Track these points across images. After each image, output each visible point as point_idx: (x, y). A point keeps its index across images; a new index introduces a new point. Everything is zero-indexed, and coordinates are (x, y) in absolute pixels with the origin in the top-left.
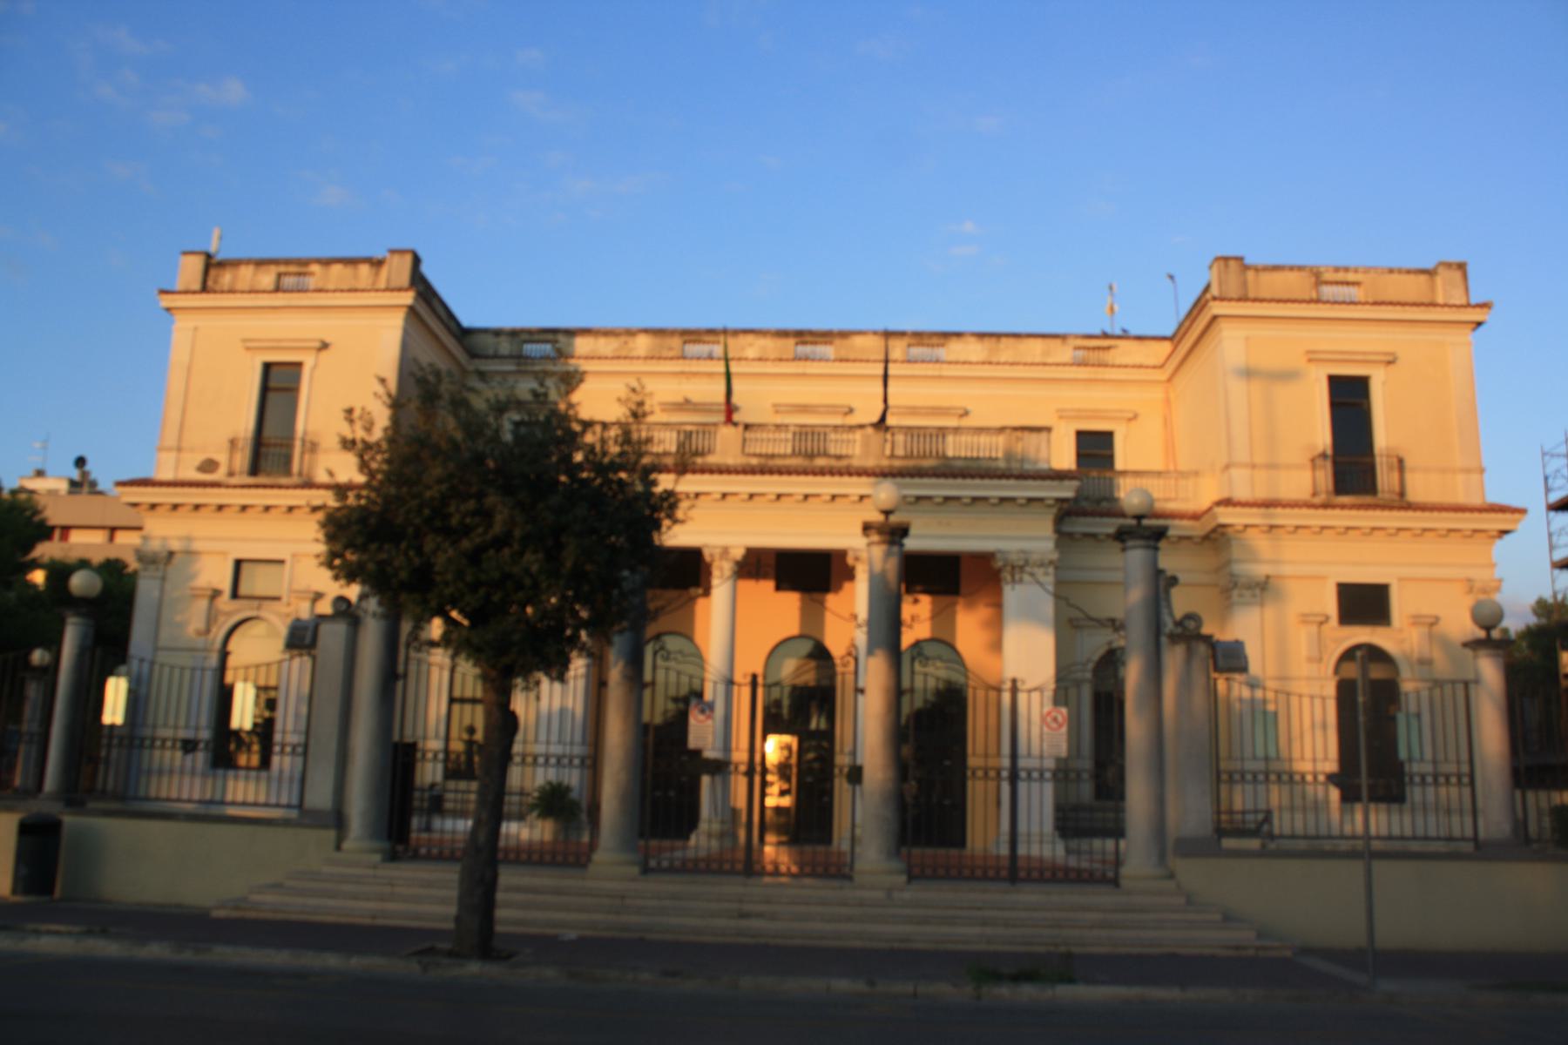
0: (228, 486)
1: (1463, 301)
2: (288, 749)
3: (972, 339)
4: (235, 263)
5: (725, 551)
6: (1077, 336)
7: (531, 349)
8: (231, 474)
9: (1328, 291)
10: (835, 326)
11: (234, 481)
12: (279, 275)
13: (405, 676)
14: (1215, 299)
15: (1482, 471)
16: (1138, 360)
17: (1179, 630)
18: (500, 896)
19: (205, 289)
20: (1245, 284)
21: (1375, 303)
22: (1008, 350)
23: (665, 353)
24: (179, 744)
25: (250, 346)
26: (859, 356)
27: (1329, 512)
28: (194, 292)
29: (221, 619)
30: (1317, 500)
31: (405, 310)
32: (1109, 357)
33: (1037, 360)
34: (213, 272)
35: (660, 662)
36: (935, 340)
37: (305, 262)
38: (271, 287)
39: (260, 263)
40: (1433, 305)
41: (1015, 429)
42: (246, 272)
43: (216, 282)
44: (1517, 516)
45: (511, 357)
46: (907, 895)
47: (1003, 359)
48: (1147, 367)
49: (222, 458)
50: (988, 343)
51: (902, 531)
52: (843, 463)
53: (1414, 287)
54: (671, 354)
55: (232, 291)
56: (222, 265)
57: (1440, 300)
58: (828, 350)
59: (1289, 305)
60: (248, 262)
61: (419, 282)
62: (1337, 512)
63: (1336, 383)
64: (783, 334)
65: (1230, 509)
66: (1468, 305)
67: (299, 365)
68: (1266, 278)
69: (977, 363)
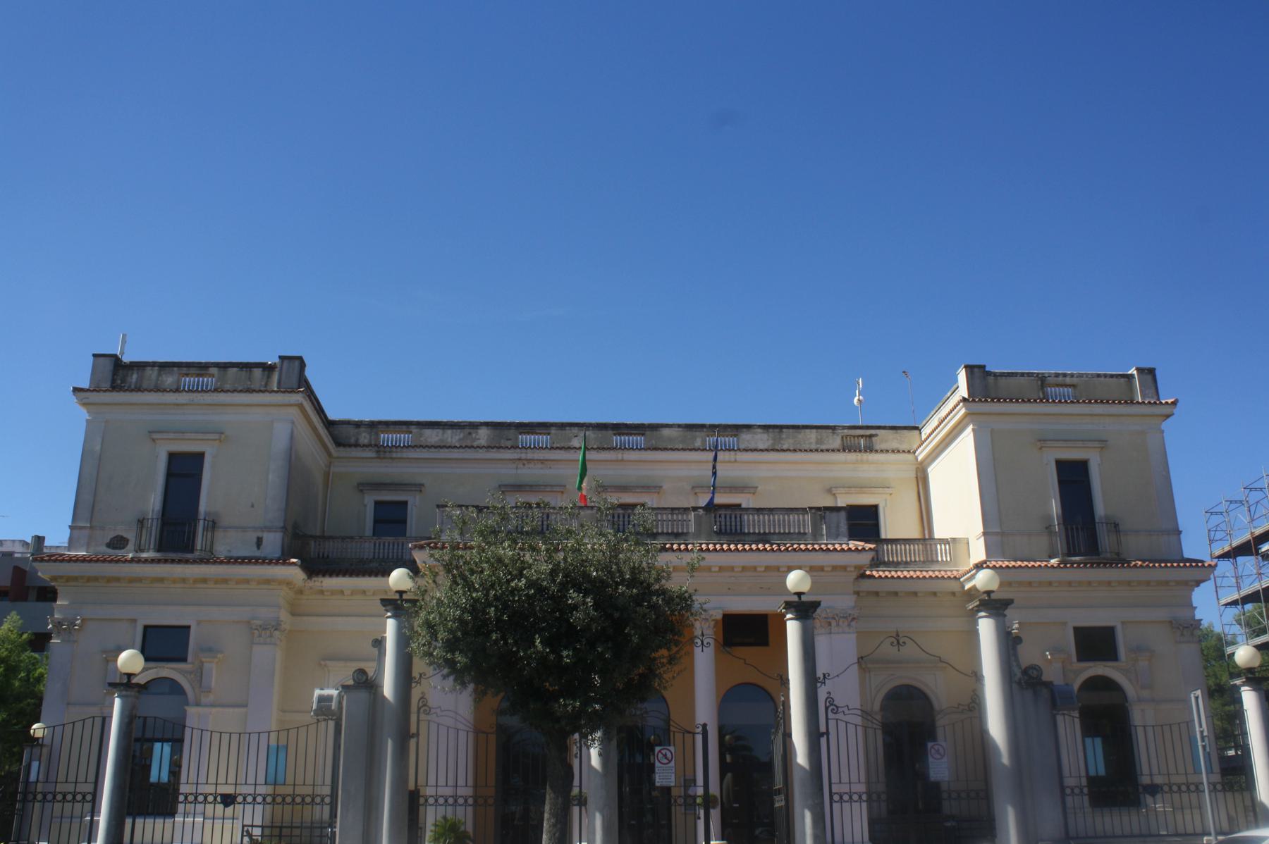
2: (259, 799)
3: (759, 430)
6: (844, 428)
7: (386, 438)
13: (417, 735)
15: (1180, 532)
22: (788, 441)
24: (219, 799)
25: (1043, 441)
33: (813, 447)
35: (831, 715)
41: (819, 509)
43: (123, 381)
45: (370, 445)
47: (785, 447)
49: (131, 536)
50: (772, 433)
55: (138, 389)
63: (1061, 465)
67: (200, 456)
68: (1002, 381)
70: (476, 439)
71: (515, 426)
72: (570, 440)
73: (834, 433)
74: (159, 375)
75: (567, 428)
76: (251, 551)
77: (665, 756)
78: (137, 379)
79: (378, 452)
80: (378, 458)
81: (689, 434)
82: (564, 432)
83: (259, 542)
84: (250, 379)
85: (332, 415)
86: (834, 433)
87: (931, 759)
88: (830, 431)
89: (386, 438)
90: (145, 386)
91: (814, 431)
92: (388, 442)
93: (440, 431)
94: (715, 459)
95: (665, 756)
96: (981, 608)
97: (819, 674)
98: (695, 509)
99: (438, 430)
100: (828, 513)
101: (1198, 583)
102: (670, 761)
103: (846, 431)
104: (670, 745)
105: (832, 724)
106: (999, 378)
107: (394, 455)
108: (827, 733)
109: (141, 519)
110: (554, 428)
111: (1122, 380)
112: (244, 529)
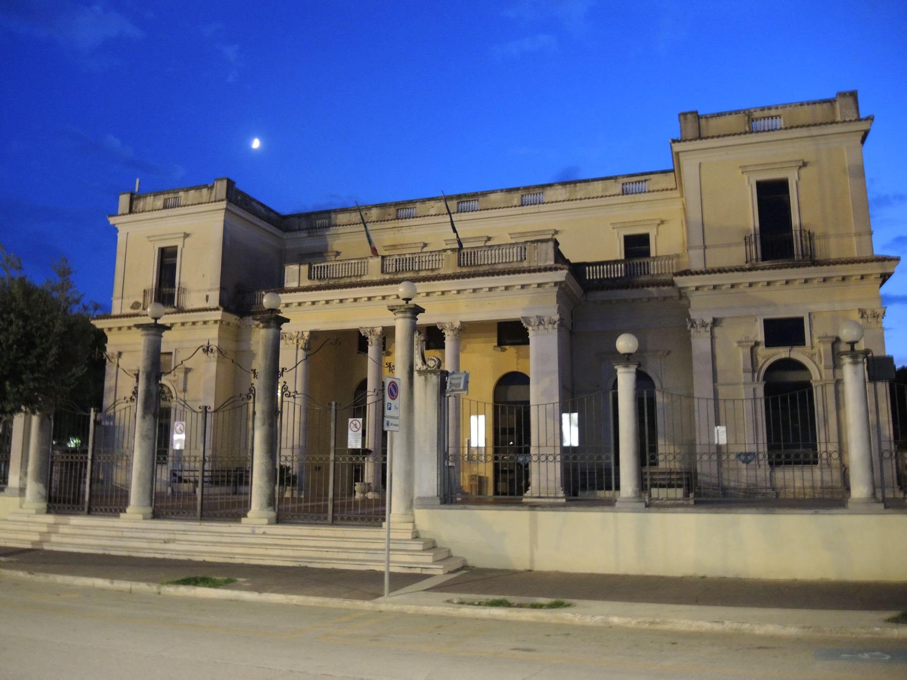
5: (372, 330)
6: (624, 176)
9: (760, 124)
10: (479, 189)
15: (871, 233)
17: (425, 367)
19: (131, 211)
23: (387, 217)
27: (754, 272)
28: (126, 214)
30: (747, 266)
31: (224, 211)
33: (600, 195)
34: (135, 203)
36: (537, 191)
40: (834, 122)
44: (893, 262)
47: (578, 197)
51: (417, 310)
52: (435, 273)
53: (820, 112)
54: (390, 217)
57: (839, 119)
59: (726, 138)
62: (759, 272)
66: (859, 120)
68: (713, 122)
69: (564, 201)
72: (428, 210)
73: (615, 182)
74: (154, 201)
76: (204, 305)
78: (143, 205)
79: (309, 233)
80: (309, 237)
82: (424, 205)
84: (201, 196)
86: (615, 182)
88: (613, 180)
90: (147, 209)
91: (601, 182)
94: (452, 222)
96: (408, 310)
98: (445, 250)
100: (539, 244)
102: (359, 429)
104: (183, 421)
105: (285, 404)
106: (709, 119)
107: (319, 234)
111: (825, 106)
112: (199, 291)
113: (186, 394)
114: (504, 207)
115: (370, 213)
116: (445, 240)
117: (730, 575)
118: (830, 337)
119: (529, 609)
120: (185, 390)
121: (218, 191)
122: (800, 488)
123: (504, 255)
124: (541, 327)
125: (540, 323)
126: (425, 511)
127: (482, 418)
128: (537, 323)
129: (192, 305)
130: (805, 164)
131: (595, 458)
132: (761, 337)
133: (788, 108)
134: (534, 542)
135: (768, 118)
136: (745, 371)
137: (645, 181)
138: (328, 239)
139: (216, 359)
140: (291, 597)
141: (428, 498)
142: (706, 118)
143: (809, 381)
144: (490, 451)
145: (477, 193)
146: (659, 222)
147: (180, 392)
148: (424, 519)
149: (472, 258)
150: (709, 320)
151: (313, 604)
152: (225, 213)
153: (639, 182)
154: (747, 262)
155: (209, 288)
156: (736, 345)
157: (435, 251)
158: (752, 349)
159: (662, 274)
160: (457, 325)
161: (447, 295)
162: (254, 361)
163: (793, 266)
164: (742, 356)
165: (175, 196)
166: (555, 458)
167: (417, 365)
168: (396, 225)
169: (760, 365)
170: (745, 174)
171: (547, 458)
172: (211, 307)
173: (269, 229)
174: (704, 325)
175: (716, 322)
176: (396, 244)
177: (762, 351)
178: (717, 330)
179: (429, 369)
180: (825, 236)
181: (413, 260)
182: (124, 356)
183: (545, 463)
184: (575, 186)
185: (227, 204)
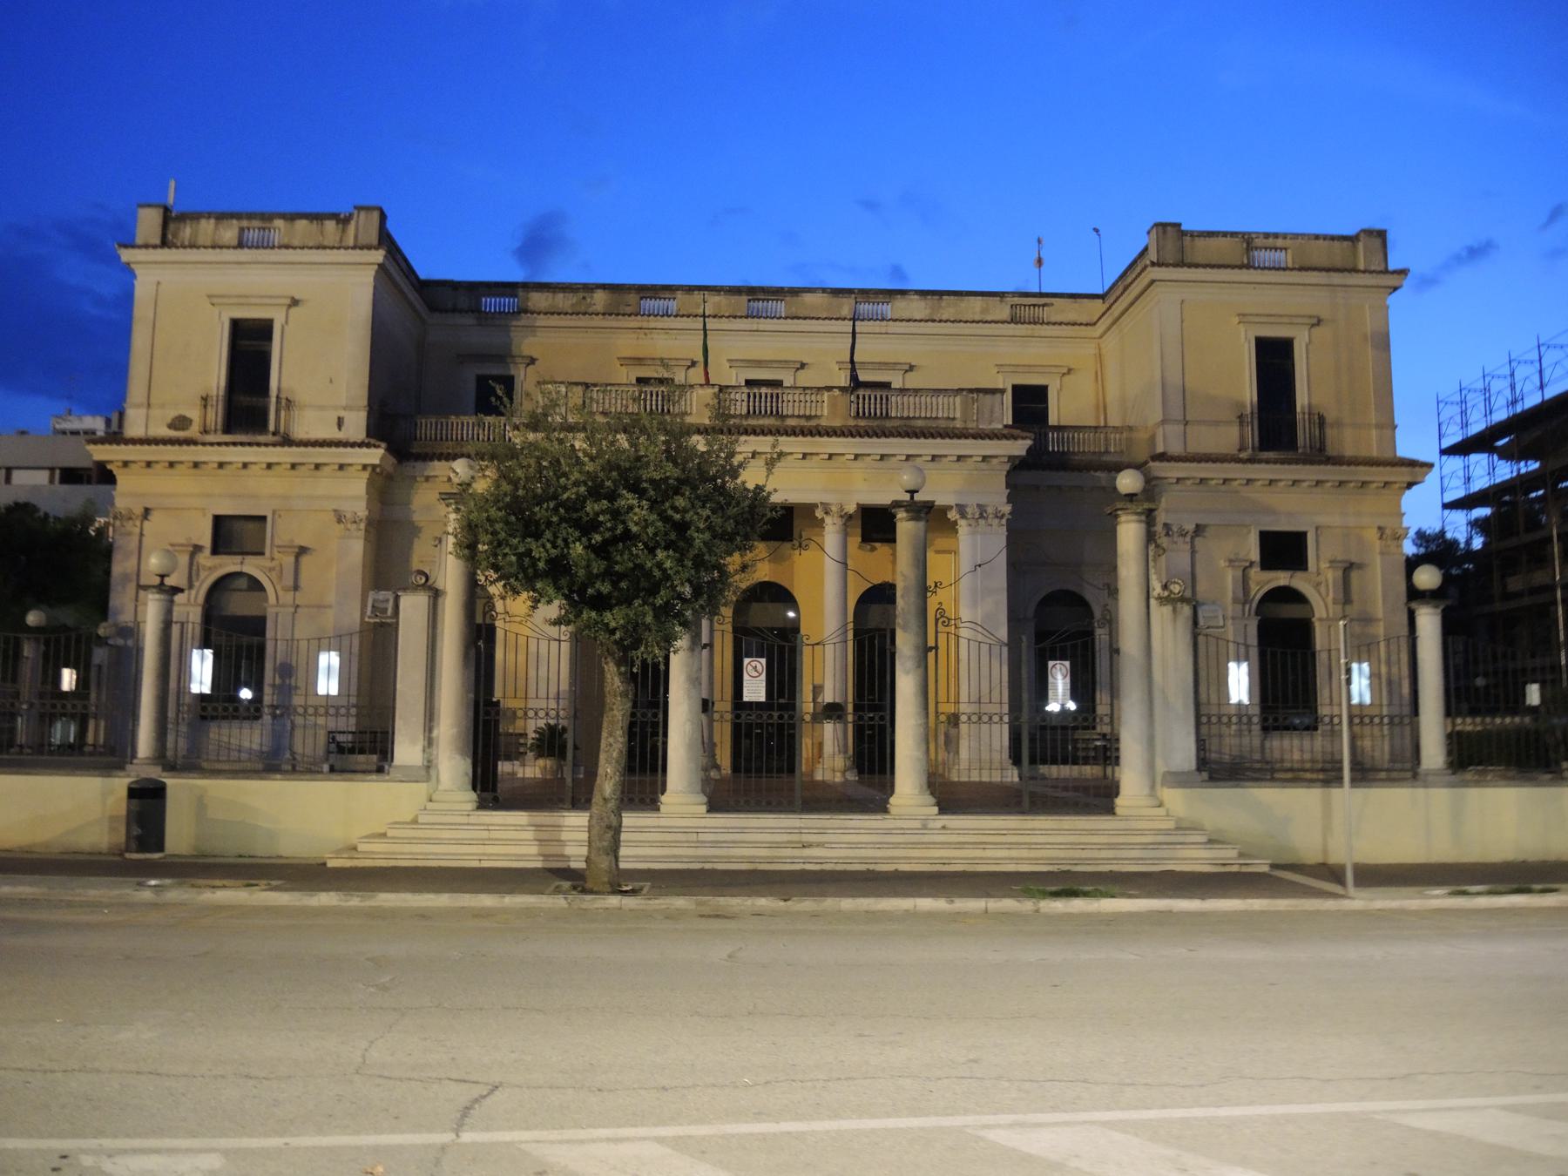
0: (204, 444)
1: (1382, 268)
3: (916, 297)
4: (196, 217)
6: (1014, 294)
8: (205, 431)
11: (210, 438)
12: (242, 230)
14: (1153, 264)
15: (1395, 427)
16: (1071, 317)
17: (1166, 593)
18: (623, 836)
19: (165, 243)
20: (1182, 250)
21: (1301, 269)
22: (949, 308)
23: (623, 309)
26: (806, 314)
28: (155, 247)
29: (203, 574)
30: (1243, 455)
31: (376, 267)
32: (1047, 314)
33: (977, 318)
34: (172, 226)
37: (267, 217)
38: (235, 242)
39: (221, 217)
40: (1355, 270)
41: (971, 391)
42: (207, 227)
43: (175, 236)
44: (1425, 469)
46: (939, 824)
47: (944, 318)
48: (1081, 324)
49: (194, 414)
52: (813, 423)
55: (193, 246)
56: (183, 218)
58: (781, 307)
59: (1222, 271)
60: (209, 215)
61: (385, 240)
62: (1263, 466)
64: (735, 291)
65: (1165, 464)
66: (1386, 271)
68: (1200, 243)
69: (921, 321)
70: (590, 305)
71: (636, 289)
73: (1001, 301)
75: (696, 292)
76: (332, 433)
77: (755, 668)
78: (191, 235)
81: (835, 301)
83: (340, 423)
85: (424, 273)
86: (1001, 301)
87: (746, 677)
89: (490, 303)
92: (490, 308)
93: (550, 295)
95: (755, 668)
97: (930, 583)
98: (829, 389)
99: (547, 294)
100: (981, 395)
101: (1410, 485)
102: (760, 674)
103: (1016, 299)
105: (942, 638)
108: (936, 648)
109: (204, 395)
110: (679, 292)
111: (1345, 244)
112: (322, 408)
113: (297, 593)
114: (826, 318)
115: (592, 297)
116: (729, 360)
117: (1552, 857)
118: (1340, 562)
119: (1538, 895)
120: (296, 588)
121: (361, 229)
122: (1298, 761)
123: (940, 407)
124: (982, 522)
125: (981, 516)
126: (1180, 791)
127: (1244, 666)
128: (977, 516)
129: (307, 433)
130: (1319, 322)
131: (765, 717)
132: (1255, 555)
133: (1300, 240)
134: (1327, 829)
135: (1281, 249)
136: (1235, 601)
137: (1044, 305)
138: (512, 334)
139: (362, 533)
140: (1250, 901)
141: (1183, 773)
142: (1192, 236)
143: (1310, 619)
144: (1256, 710)
145: (782, 288)
146: (1065, 370)
147: (286, 589)
148: (1177, 801)
149: (872, 406)
150: (1190, 527)
151: (1281, 909)
152: (377, 272)
153: (1034, 305)
154: (1240, 450)
155: (344, 403)
156: (1223, 563)
157: (811, 388)
158: (1244, 570)
159: (1079, 452)
160: (851, 508)
161: (836, 461)
162: (416, 540)
163: (1297, 462)
164: (1230, 578)
165: (264, 225)
166: (1001, 719)
167: (1154, 589)
168: (645, 325)
169: (1253, 593)
170: (1241, 325)
171: (990, 718)
172: (351, 440)
173: (418, 306)
174: (1183, 534)
175: (1199, 530)
176: (641, 356)
177: (1256, 574)
178: (1198, 541)
179: (1172, 596)
180: (1339, 424)
181: (778, 397)
182: (154, 516)
183: (999, 725)
184: (941, 299)
185: (385, 257)
